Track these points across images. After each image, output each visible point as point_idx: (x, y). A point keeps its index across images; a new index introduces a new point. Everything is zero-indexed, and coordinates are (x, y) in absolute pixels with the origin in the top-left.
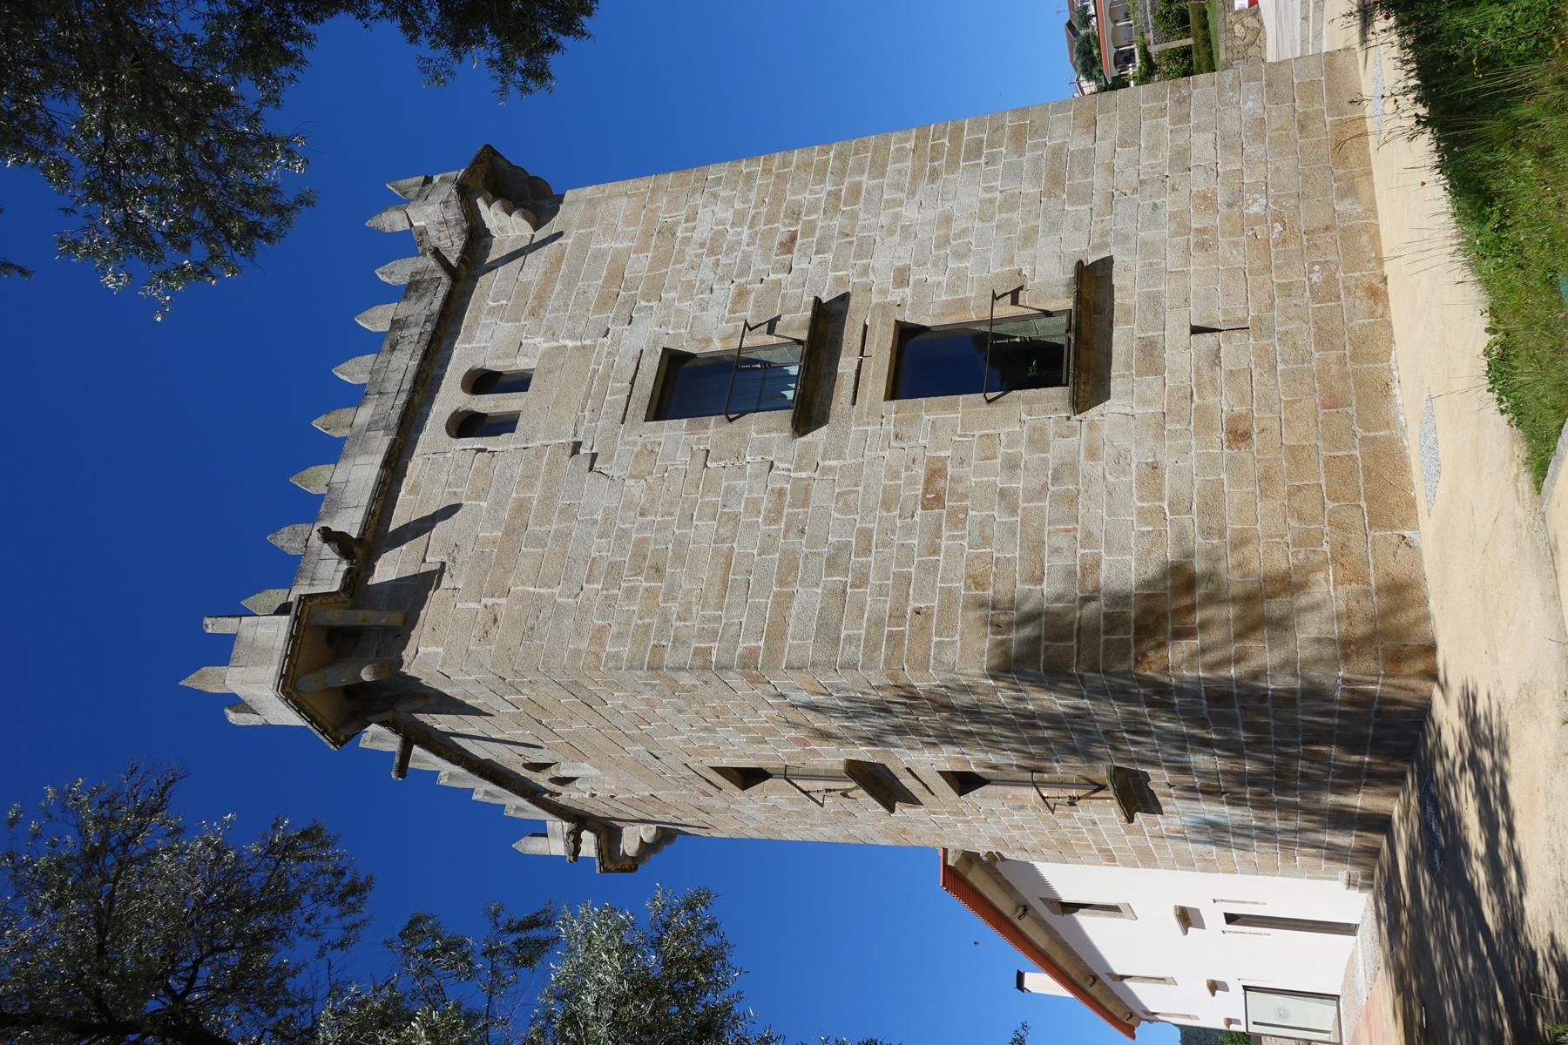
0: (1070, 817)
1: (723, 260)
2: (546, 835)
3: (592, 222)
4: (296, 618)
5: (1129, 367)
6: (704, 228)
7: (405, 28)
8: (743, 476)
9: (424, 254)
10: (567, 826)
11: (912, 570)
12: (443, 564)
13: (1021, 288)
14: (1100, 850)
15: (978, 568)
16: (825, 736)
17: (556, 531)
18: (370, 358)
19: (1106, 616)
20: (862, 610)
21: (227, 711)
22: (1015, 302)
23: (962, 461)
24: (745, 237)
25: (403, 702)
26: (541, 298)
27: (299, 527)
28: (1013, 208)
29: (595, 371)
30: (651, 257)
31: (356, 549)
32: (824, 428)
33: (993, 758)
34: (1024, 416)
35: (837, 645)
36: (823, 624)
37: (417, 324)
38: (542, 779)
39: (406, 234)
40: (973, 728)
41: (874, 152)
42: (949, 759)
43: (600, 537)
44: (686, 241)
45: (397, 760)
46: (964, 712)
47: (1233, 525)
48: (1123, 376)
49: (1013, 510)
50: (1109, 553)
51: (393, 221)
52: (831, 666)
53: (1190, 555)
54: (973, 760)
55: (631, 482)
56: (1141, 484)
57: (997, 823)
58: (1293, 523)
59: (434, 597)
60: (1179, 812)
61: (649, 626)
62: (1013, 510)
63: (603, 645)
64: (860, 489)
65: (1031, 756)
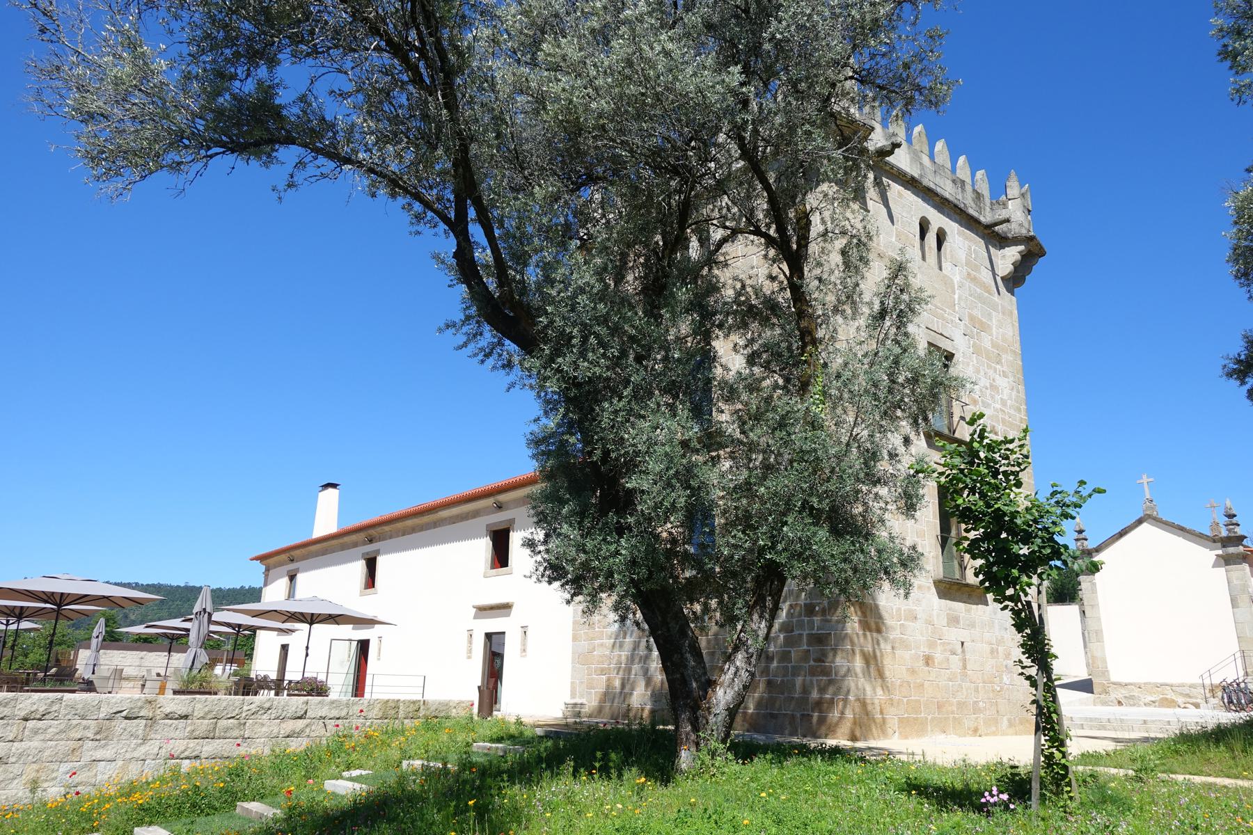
1: (988, 392)
3: (1004, 313)
51: (1014, 189)
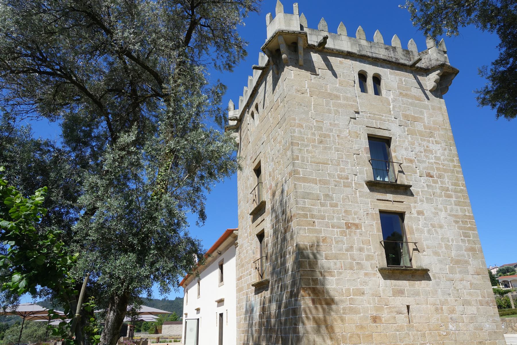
0: (252, 267)
1: (422, 154)
3: (433, 109)
4: (300, 33)
5: (395, 286)
6: (433, 147)
7: (496, 61)
8: (352, 166)
9: (419, 54)
10: (238, 116)
11: (326, 220)
12: (318, 75)
13: (419, 252)
14: (241, 276)
15: (328, 240)
16: (274, 195)
18: (383, 41)
19: (317, 279)
20: (313, 205)
22: (414, 250)
23: (361, 234)
24: (431, 161)
26: (406, 95)
27: (327, 27)
28: (446, 248)
29: (383, 116)
30: (423, 128)
32: (369, 191)
33: (270, 245)
34: (376, 253)
35: (303, 198)
36: (309, 194)
37: (395, 55)
38: (253, 108)
39: (426, 48)
40: (279, 239)
41: (464, 202)
42: (268, 232)
44: (429, 141)
46: (284, 237)
47: (347, 317)
48: (392, 284)
49: (347, 250)
50: (335, 280)
52: (296, 197)
53: (337, 304)
54: (269, 238)
55: (348, 131)
56: (357, 289)
57: (247, 245)
58: (349, 335)
59: (308, 73)
60: (256, 300)
61: (304, 141)
62: (347, 250)
63: (297, 127)
64: (350, 203)
65: (271, 256)
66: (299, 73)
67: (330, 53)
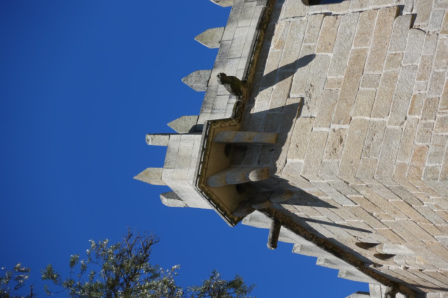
2: (368, 294)
4: (206, 137)
10: (385, 289)
12: (302, 99)
17: (385, 74)
21: (161, 197)
25: (273, 195)
27: (202, 72)
31: (242, 88)
38: (369, 254)
43: (419, 79)
45: (270, 235)
59: (297, 122)
63: (423, 161)
66: (292, 146)
67: (257, 70)
